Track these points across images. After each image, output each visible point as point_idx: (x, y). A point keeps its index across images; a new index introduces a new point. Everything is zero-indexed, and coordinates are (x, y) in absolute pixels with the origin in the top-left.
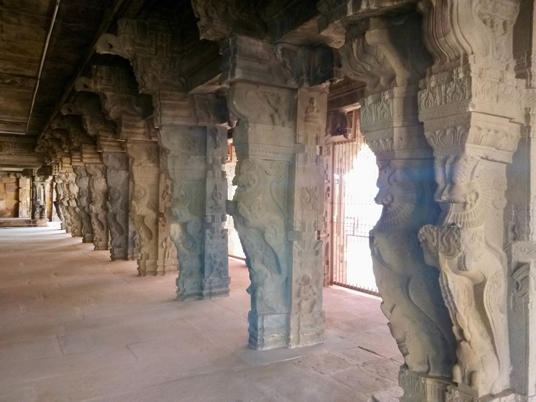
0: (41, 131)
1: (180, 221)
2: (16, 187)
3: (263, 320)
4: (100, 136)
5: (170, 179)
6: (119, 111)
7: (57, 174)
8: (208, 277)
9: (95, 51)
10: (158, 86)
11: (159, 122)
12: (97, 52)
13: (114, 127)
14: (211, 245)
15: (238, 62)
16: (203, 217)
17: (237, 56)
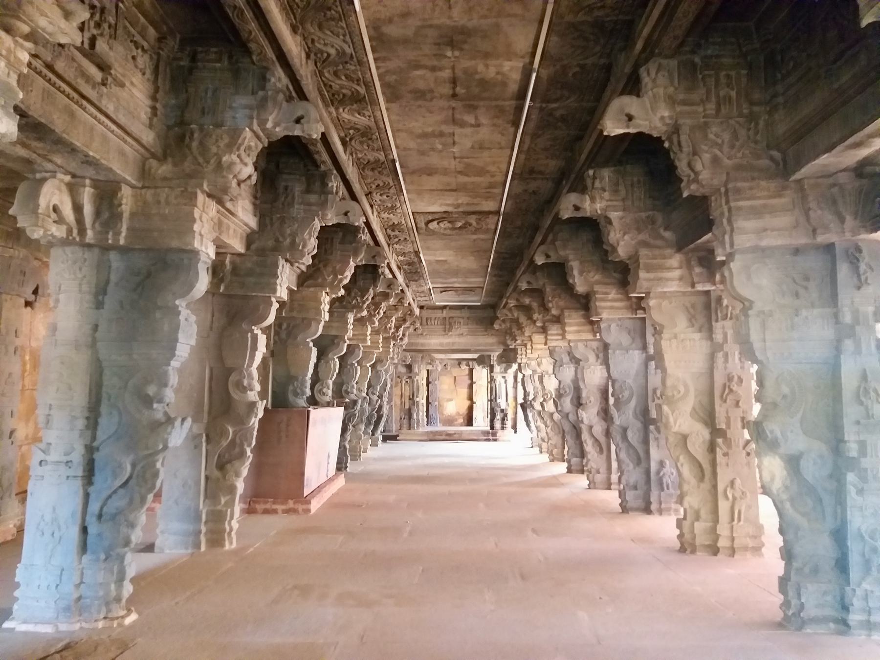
0: (501, 298)
1: (782, 450)
2: (469, 382)
4: (595, 293)
6: (633, 242)
7: (524, 361)
8: (859, 585)
9: (602, 131)
10: (725, 175)
11: (728, 246)
12: (605, 133)
13: (623, 274)
14: (861, 509)
16: (837, 444)
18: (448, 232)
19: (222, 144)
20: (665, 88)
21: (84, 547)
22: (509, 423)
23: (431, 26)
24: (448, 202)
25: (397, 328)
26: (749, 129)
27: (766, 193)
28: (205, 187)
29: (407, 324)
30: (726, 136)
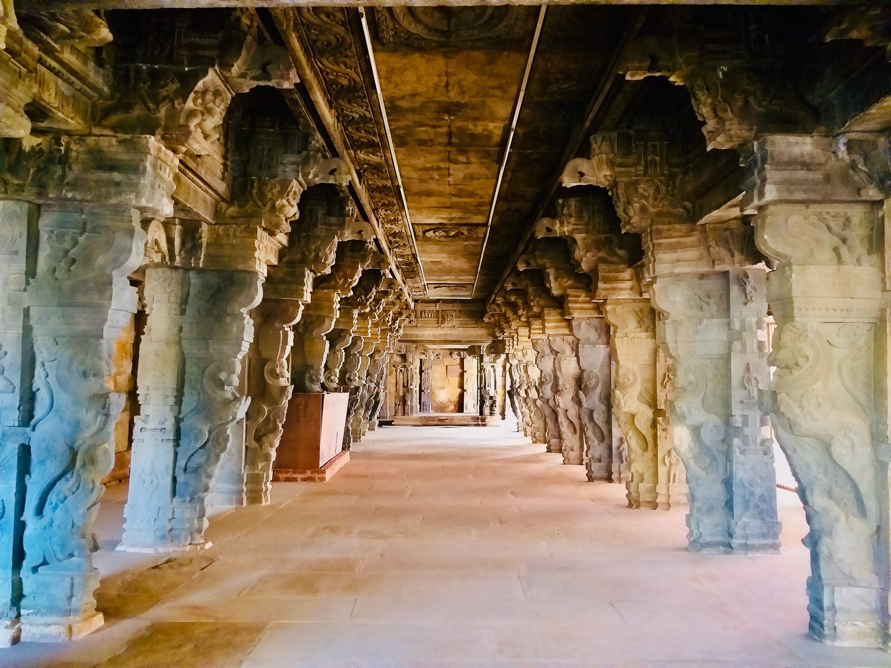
0: (490, 293)
1: (688, 422)
2: (461, 371)
3: (833, 594)
4: (568, 295)
5: (671, 357)
6: (594, 259)
7: (512, 351)
8: (740, 519)
9: (561, 184)
11: (651, 272)
13: (588, 282)
14: (743, 464)
15: (768, 176)
16: (727, 418)
17: (767, 166)
18: (443, 239)
19: (275, 191)
20: (607, 154)
21: (174, 493)
22: (497, 410)
23: (433, 102)
24: (443, 216)
25: (394, 321)
26: (668, 186)
27: (679, 234)
28: (263, 225)
29: (403, 317)
30: (651, 191)
